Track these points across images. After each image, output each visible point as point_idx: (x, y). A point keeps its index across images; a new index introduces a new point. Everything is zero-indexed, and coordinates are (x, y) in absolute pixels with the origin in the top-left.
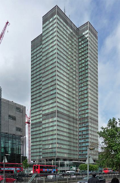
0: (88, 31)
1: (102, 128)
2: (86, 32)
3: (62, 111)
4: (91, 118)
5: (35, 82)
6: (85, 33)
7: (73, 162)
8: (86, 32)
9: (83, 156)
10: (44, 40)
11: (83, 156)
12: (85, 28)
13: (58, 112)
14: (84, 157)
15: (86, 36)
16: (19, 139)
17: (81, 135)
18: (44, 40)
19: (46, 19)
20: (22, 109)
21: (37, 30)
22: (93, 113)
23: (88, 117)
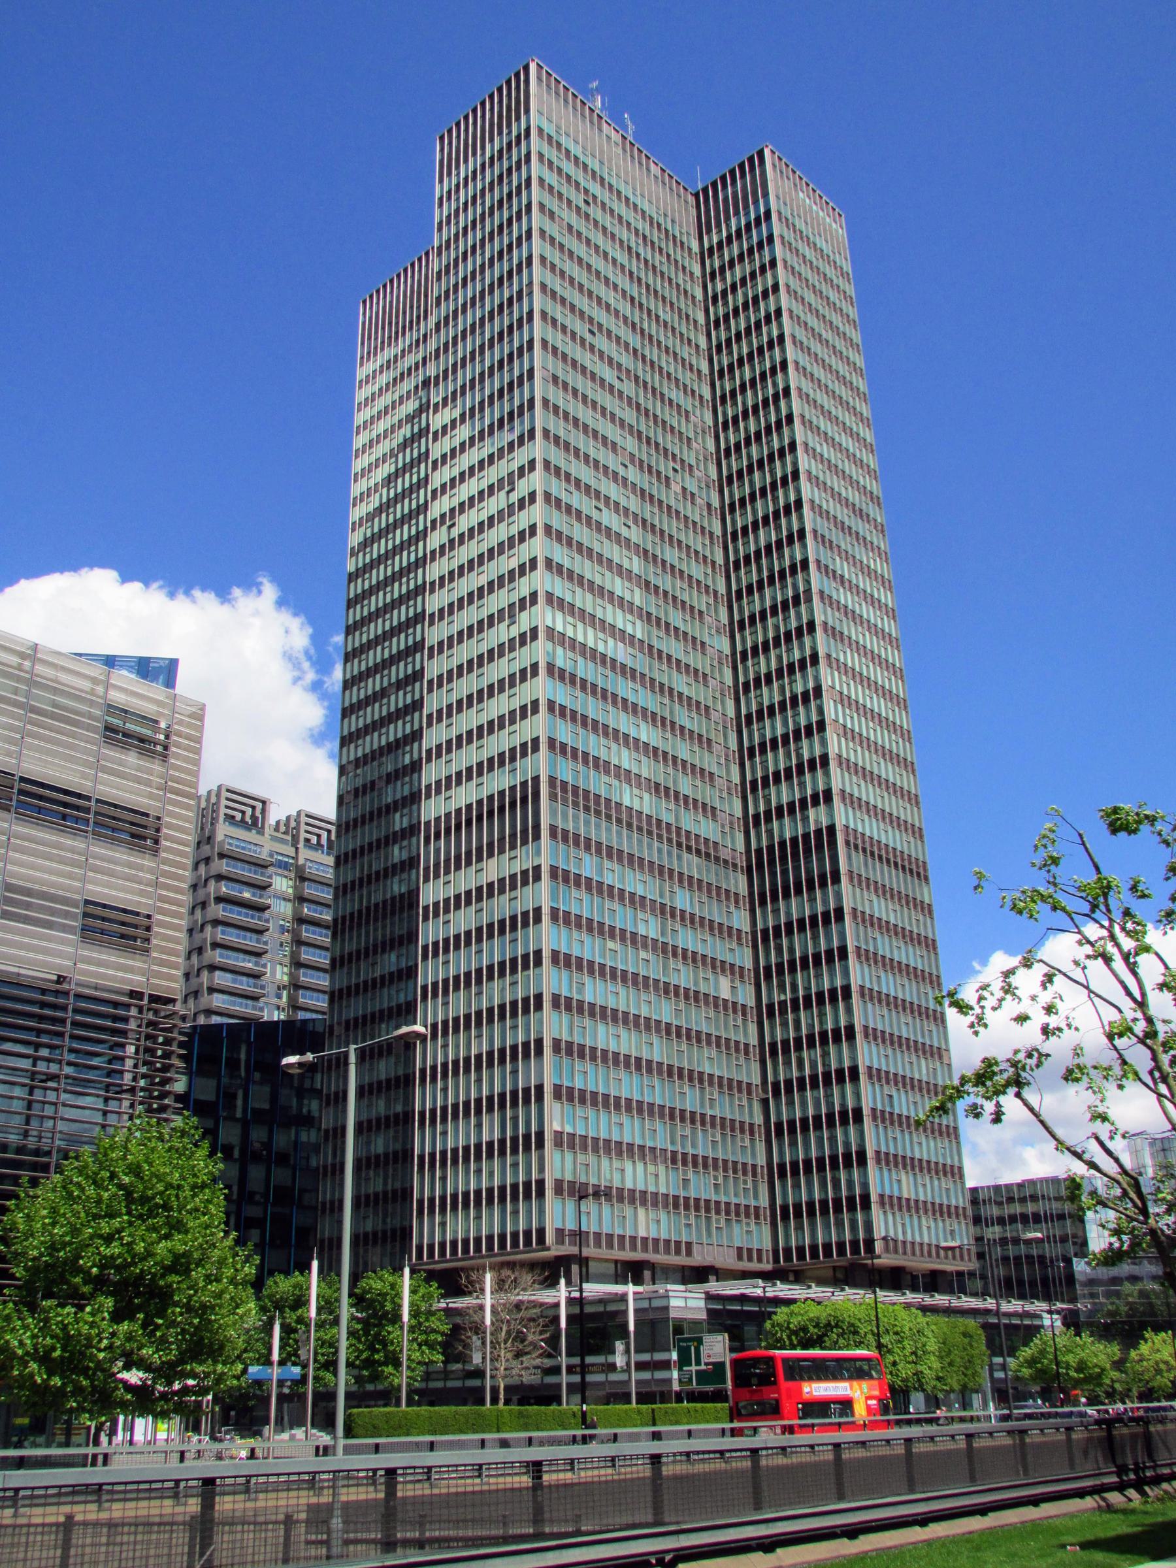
23: (831, 829)
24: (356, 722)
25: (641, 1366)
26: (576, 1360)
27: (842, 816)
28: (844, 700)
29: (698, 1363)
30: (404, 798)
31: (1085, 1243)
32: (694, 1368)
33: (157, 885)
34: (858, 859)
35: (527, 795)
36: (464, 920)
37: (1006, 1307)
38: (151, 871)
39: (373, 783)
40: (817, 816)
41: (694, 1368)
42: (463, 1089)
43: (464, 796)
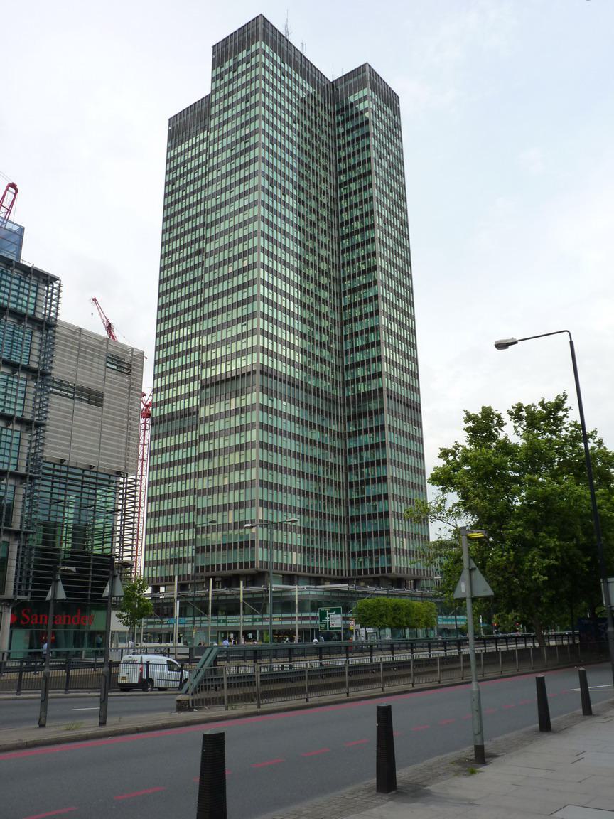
0: (366, 91)
2: (361, 94)
4: (394, 397)
10: (215, 115)
13: (265, 372)
18: (215, 115)
19: (225, 52)
23: (381, 390)
26: (237, 597)
40: (374, 384)
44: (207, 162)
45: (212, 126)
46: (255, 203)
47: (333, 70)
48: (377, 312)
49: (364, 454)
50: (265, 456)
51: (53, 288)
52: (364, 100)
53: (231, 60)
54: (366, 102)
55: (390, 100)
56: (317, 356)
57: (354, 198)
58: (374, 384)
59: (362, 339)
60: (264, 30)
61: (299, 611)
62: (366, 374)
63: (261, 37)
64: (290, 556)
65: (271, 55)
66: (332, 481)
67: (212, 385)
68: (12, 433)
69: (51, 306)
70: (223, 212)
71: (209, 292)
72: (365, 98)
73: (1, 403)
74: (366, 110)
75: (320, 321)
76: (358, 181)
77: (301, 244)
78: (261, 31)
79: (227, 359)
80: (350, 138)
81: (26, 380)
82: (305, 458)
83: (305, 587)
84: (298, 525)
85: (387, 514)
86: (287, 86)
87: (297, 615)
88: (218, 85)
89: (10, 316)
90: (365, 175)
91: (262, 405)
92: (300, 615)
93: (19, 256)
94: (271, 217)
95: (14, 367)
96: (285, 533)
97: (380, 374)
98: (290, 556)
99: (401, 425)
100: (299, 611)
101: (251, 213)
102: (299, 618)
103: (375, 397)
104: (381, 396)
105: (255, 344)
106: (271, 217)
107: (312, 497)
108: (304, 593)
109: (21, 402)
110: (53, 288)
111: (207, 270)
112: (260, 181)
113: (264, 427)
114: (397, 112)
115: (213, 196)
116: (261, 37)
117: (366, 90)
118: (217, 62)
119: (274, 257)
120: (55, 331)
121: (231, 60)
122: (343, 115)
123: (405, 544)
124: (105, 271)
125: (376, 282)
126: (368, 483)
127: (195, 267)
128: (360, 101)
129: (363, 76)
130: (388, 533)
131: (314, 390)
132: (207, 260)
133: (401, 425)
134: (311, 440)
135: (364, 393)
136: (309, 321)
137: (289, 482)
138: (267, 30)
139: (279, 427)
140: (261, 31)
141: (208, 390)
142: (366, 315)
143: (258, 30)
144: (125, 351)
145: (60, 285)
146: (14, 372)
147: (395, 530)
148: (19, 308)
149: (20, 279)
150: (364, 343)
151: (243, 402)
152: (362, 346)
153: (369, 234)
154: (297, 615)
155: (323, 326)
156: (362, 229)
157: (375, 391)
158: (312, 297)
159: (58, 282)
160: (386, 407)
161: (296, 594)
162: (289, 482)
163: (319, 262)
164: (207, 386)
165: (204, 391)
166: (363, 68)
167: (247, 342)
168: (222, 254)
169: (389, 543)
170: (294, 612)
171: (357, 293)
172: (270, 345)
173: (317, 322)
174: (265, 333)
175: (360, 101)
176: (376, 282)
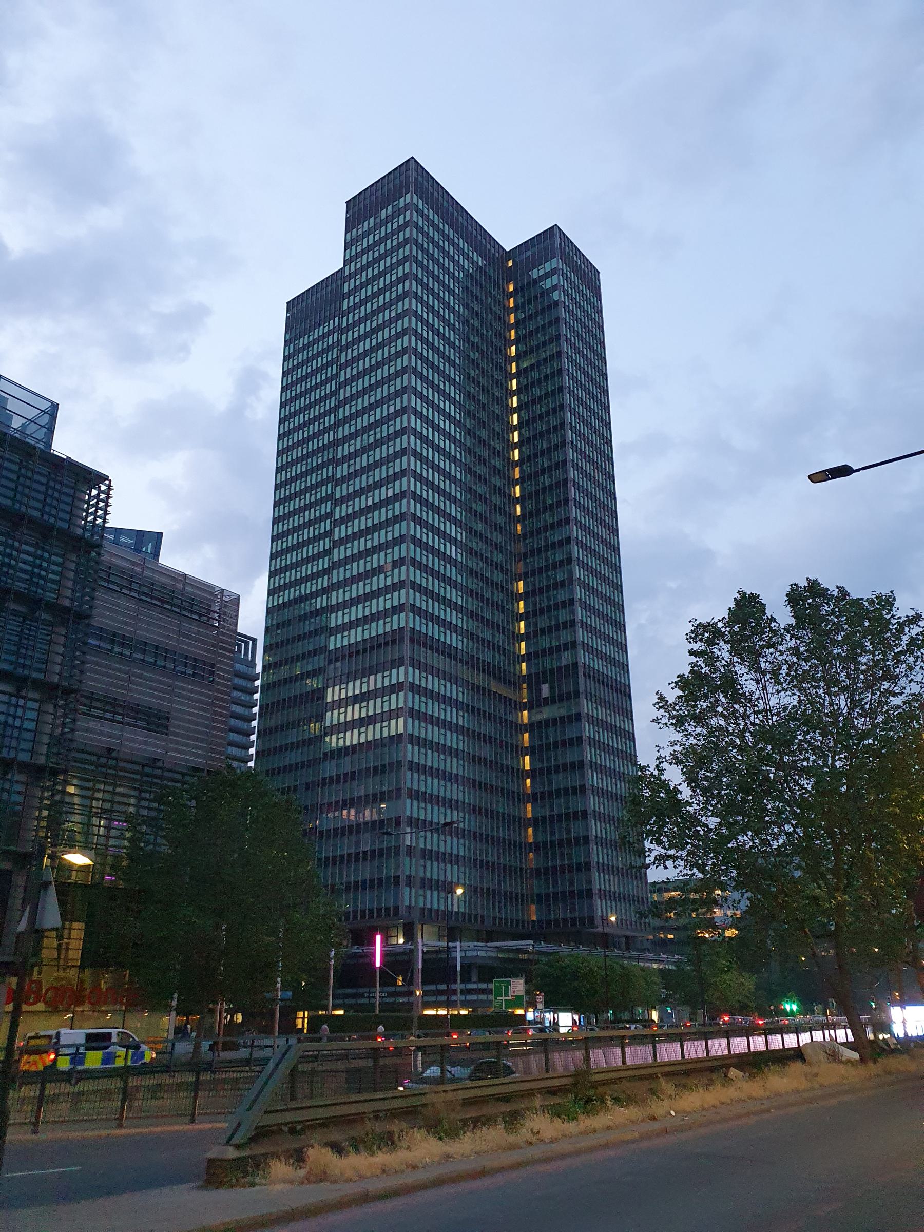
0: (554, 263)
1: (666, 867)
2: (548, 267)
3: (434, 631)
4: (591, 674)
5: (292, 540)
6: (542, 272)
7: (499, 949)
8: (548, 267)
9: (554, 854)
10: (349, 293)
11: (554, 854)
12: (533, 254)
13: (418, 639)
14: (562, 859)
15: (548, 284)
16: (184, 783)
17: (546, 869)
18: (349, 293)
19: (360, 210)
20: (217, 609)
21: (321, 253)
22: (594, 582)
23: (575, 665)
24: (279, 581)
25: (490, 992)
26: (372, 1001)
27: (583, 657)
28: (586, 586)
29: (507, 995)
30: (310, 632)
31: (7, 870)
32: (503, 998)
33: (212, 704)
34: (591, 685)
35: (395, 638)
36: (353, 713)
37: (96, 1133)
38: (208, 696)
39: (289, 620)
40: (566, 658)
41: (503, 998)
42: (455, 848)
43: (356, 636)
44: (337, 375)
45: (345, 307)
46: (403, 495)
47: (509, 237)
48: (569, 560)
49: (551, 730)
50: (416, 702)
51: (100, 492)
52: (550, 274)
53: (372, 220)
54: (555, 277)
55: (588, 277)
56: (488, 642)
57: (538, 442)
58: (566, 658)
59: (549, 618)
60: (417, 179)
61: (462, 981)
62: (554, 644)
63: (412, 188)
64: (449, 842)
65: (426, 211)
66: (508, 791)
67: (344, 657)
68: (11, 786)
69: (99, 500)
70: (359, 423)
71: (346, 411)
72: (554, 272)
73: (2, 708)
74: (555, 288)
75: (492, 573)
76: (554, 613)
77: (469, 470)
78: (412, 179)
79: (363, 722)
80: (534, 343)
81: (40, 701)
82: (472, 573)
83: (472, 944)
84: (461, 825)
85: (586, 840)
86: (446, 254)
87: (459, 986)
88: (353, 253)
89: (14, 602)
90: (554, 410)
91: (412, 685)
92: (462, 986)
93: (49, 445)
94: (425, 411)
95: (20, 682)
96: (442, 865)
97: (574, 644)
98: (449, 842)
99: (602, 713)
100: (462, 981)
101: (397, 508)
102: (462, 991)
103: (567, 676)
104: (576, 674)
105: (401, 730)
106: (425, 411)
107: (481, 840)
108: (469, 954)
109: (33, 715)
110: (100, 492)
111: (336, 544)
112: (411, 250)
113: (413, 714)
114: (596, 290)
115: (345, 440)
116: (412, 188)
117: (554, 261)
118: (350, 225)
119: (430, 464)
120: (89, 625)
121: (372, 220)
122: (523, 296)
123: (612, 884)
124: (186, 474)
125: (568, 521)
126: (557, 771)
127: (321, 519)
128: (548, 275)
129: (551, 243)
130: (588, 866)
131: (483, 666)
132: (338, 508)
133: (602, 713)
134: (479, 734)
135: (552, 670)
136: (477, 594)
137: (448, 765)
138: (420, 179)
139: (436, 765)
140: (412, 179)
141: (338, 664)
142: (556, 605)
143: (407, 178)
144: (212, 594)
145: (109, 487)
146: (19, 689)
147: (598, 863)
148: (46, 517)
149: (36, 546)
150: (553, 623)
151: (387, 680)
152: (550, 628)
153: (557, 456)
154: (459, 986)
155: (496, 599)
156: (550, 467)
157: (567, 666)
158: (482, 580)
159: (107, 482)
160: (582, 689)
161: (458, 955)
162: (448, 765)
163: (490, 494)
164: (337, 660)
165: (332, 666)
166: (553, 233)
167: (392, 598)
168: (358, 480)
169: (589, 882)
170: (455, 982)
171: (543, 535)
172: (424, 680)
173: (488, 595)
174: (418, 477)
175: (548, 275)
176: (568, 521)
